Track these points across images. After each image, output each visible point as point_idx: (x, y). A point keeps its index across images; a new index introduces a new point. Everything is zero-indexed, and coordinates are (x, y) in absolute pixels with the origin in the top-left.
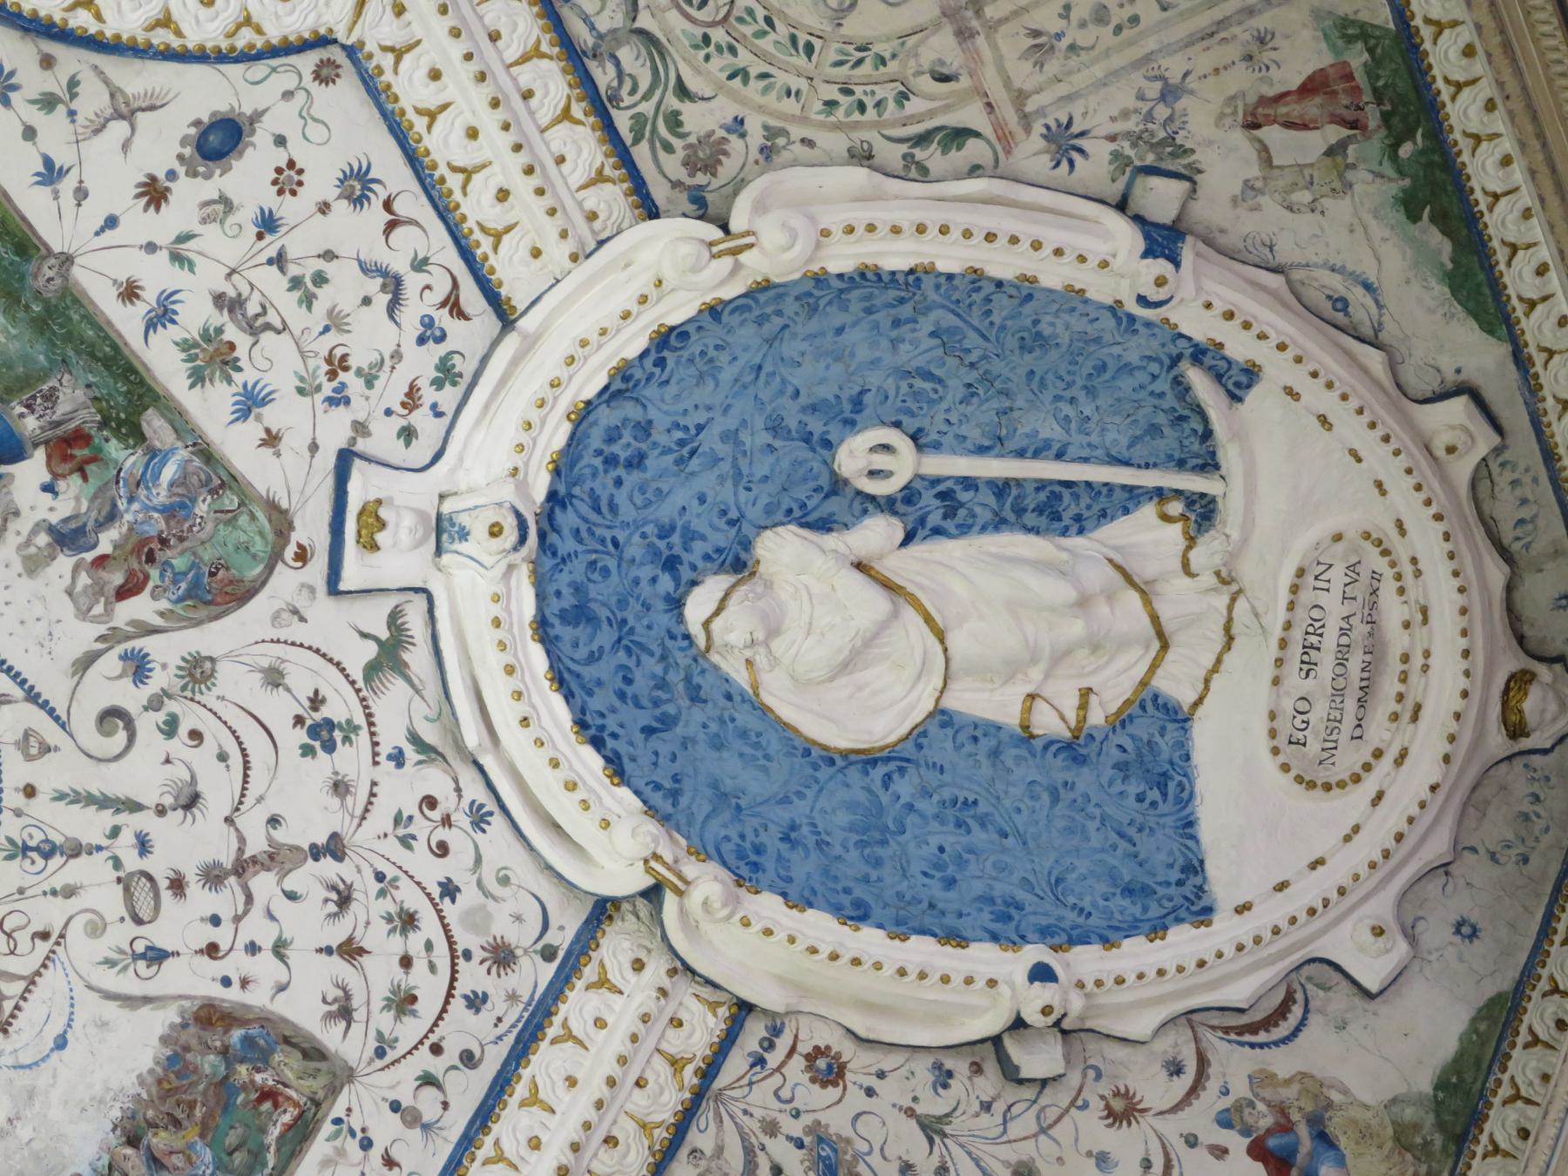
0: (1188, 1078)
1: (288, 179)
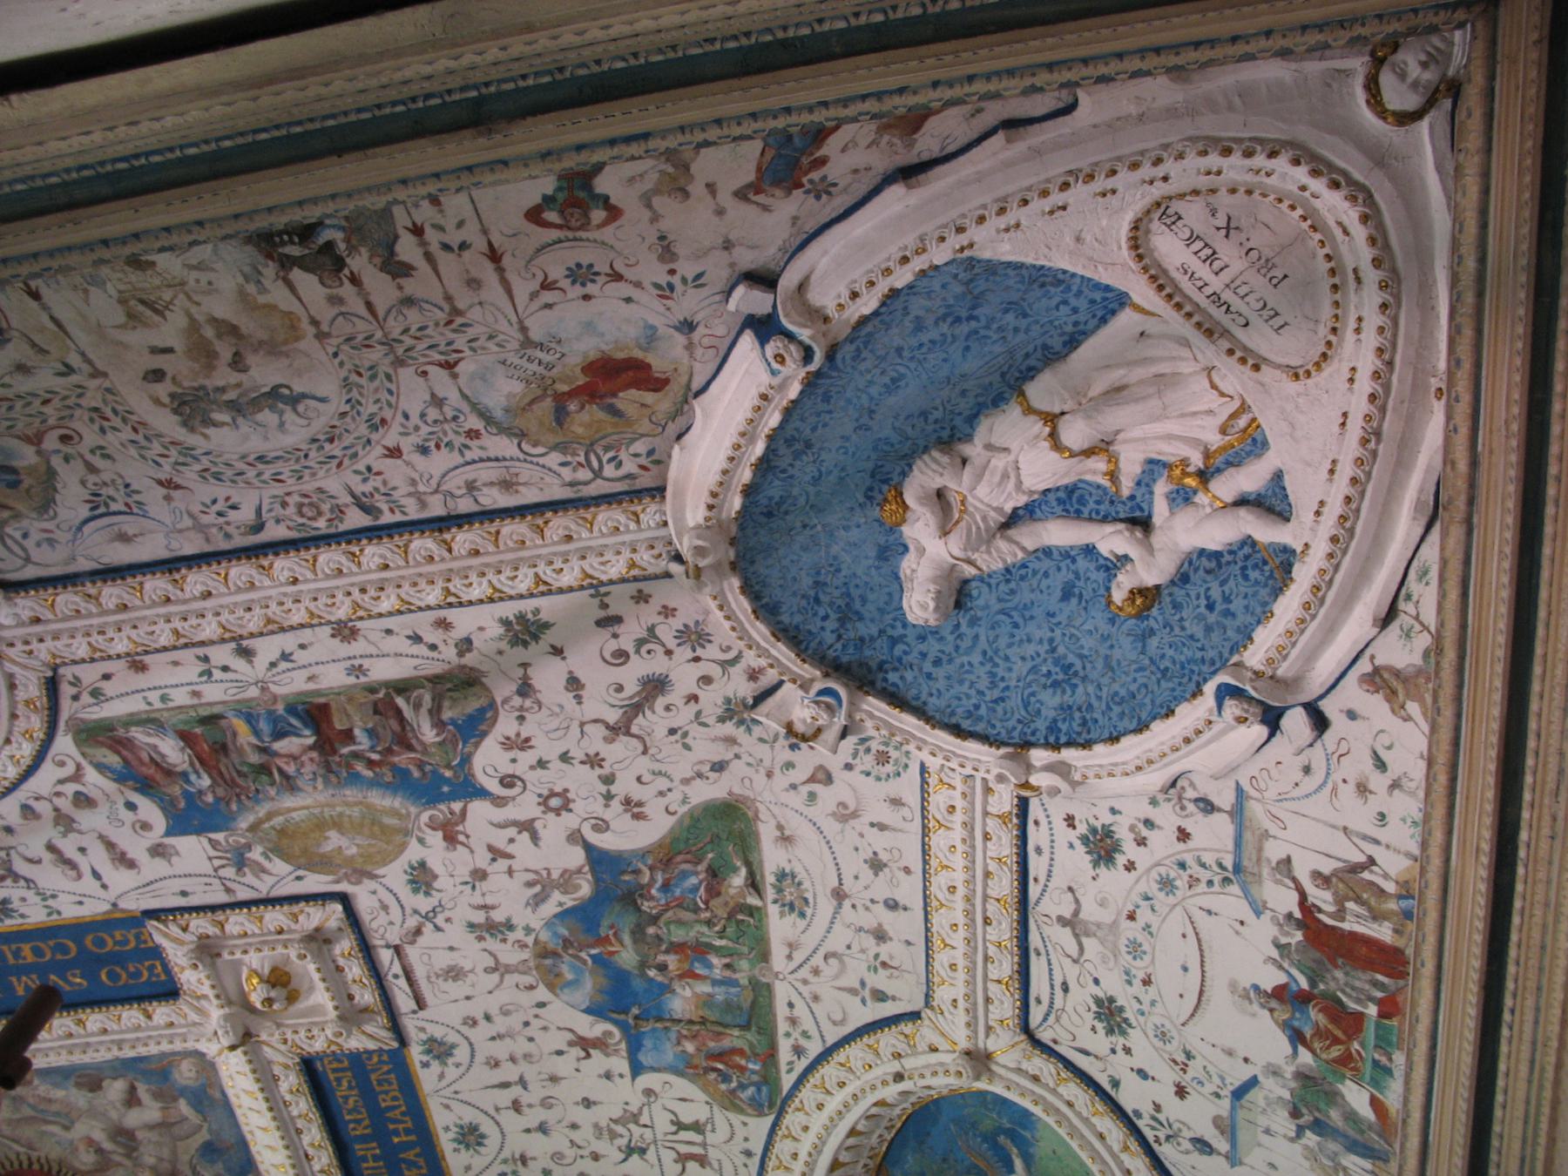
0: (462, 1069)
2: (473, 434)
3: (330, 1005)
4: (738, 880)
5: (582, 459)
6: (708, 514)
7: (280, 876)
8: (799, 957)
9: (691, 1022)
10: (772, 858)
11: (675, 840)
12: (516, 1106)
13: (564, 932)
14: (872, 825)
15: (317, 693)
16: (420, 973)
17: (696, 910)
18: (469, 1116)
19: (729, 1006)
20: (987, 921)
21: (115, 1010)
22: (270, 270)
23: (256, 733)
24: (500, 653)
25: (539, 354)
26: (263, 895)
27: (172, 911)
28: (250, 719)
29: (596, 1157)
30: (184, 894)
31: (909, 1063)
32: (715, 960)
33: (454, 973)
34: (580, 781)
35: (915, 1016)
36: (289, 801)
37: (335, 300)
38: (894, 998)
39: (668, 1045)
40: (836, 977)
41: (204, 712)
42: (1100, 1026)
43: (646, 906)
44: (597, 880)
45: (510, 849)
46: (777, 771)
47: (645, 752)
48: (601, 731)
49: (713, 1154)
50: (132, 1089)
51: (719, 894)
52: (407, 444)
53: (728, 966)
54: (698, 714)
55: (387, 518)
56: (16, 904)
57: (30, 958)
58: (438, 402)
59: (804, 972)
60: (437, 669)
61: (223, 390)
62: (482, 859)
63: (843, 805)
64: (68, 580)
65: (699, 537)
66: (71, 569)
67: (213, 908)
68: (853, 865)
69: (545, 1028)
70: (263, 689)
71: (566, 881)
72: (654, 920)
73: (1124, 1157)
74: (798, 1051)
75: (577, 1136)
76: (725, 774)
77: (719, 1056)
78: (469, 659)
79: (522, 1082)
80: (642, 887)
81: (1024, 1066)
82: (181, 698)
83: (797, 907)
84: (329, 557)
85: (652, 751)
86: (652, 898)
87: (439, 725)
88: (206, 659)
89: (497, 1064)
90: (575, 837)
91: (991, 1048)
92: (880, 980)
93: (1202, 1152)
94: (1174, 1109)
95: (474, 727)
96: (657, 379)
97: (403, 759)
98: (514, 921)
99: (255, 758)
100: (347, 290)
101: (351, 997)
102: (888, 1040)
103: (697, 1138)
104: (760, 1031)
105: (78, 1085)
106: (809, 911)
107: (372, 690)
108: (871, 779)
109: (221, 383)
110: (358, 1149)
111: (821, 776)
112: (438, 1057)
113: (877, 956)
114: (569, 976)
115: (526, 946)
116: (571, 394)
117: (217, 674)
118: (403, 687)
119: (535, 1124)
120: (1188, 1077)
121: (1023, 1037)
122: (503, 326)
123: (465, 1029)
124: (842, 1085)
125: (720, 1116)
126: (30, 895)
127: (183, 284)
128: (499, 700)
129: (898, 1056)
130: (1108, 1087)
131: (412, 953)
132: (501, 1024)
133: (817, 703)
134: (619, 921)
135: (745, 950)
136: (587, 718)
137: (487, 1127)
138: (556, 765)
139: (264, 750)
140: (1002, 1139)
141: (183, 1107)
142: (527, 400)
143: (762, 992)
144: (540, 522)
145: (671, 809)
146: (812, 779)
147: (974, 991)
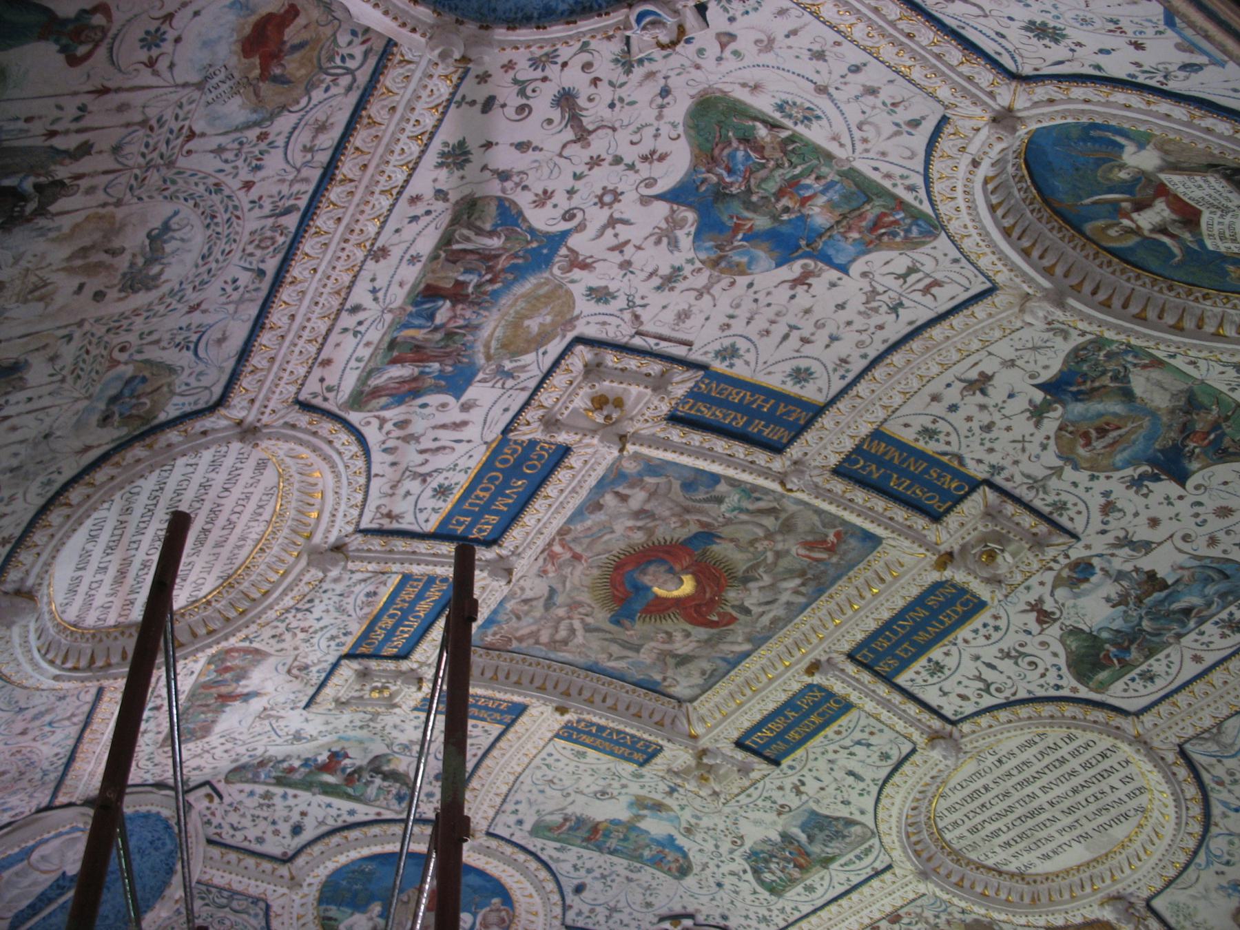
0: (753, 350)
1: (276, 833)
2: (262, 137)
3: (641, 388)
4: (762, 131)
5: (329, 78)
6: (420, 32)
7: (534, 363)
8: (846, 140)
9: (838, 222)
10: (763, 103)
11: (699, 146)
12: (805, 341)
13: (709, 244)
14: (787, 36)
15: (414, 286)
16: (666, 332)
17: (763, 166)
18: (788, 367)
19: (847, 198)
20: (909, 36)
21: (554, 479)
22: (42, 222)
23: (420, 327)
24: (463, 178)
25: (216, 80)
26: (541, 375)
27: (512, 422)
28: (406, 326)
29: (881, 327)
30: (506, 410)
31: (973, 148)
32: (808, 181)
33: (683, 316)
34: (602, 177)
35: (944, 120)
36: (485, 333)
37: (91, 190)
38: (923, 118)
39: (842, 244)
40: (879, 134)
41: (385, 345)
42: (1047, 41)
43: (734, 190)
44: (690, 206)
45: (622, 239)
46: (699, 61)
47: (614, 129)
48: (577, 147)
49: (939, 276)
50: (617, 494)
51: (763, 147)
52: (245, 175)
53: (818, 178)
54: (611, 84)
55: (303, 203)
56: (447, 483)
57: (487, 495)
58: (220, 150)
59: (860, 147)
60: (446, 219)
61: (132, 265)
62: (616, 258)
63: (757, 42)
64: (234, 377)
65: (432, 49)
66: (228, 371)
67: (527, 404)
68: (809, 67)
69: (769, 293)
70: (390, 311)
71: (674, 222)
72: (749, 191)
73: (1154, 108)
74: (911, 188)
75: (855, 327)
76: (675, 92)
77: (876, 225)
78: (454, 197)
79: (793, 328)
80: (718, 184)
81: (1035, 99)
82: (365, 353)
83: (809, 116)
84: (309, 245)
85: (617, 125)
86: (732, 184)
87: (492, 234)
88: (345, 330)
89: (768, 332)
90: (645, 201)
91: (1006, 104)
92: (903, 115)
93: (1196, 71)
94: (1148, 59)
95: (509, 216)
96: (287, 12)
97: (502, 263)
98: (677, 264)
99: (438, 336)
100: (84, 183)
101: (648, 375)
102: (946, 144)
103: (920, 275)
104: (879, 195)
105: (591, 513)
106: (819, 113)
107: (434, 257)
108: (752, 14)
109: (127, 264)
110: (753, 429)
111: (724, 39)
112: (732, 356)
113: (884, 104)
114: (745, 260)
115: (700, 270)
116: (265, 68)
117: (362, 329)
118: (446, 240)
119: (827, 341)
120: (1130, 34)
121: (1014, 84)
122: (175, 97)
123: (727, 333)
124: (953, 189)
125: (917, 255)
126: (445, 474)
127: (28, 270)
128: (500, 194)
129: (963, 149)
130: (1097, 73)
131: (648, 327)
132: (743, 313)
133: (644, 28)
134: (727, 213)
135: (815, 162)
136: (558, 149)
137: (803, 364)
138: (578, 185)
139: (436, 329)
140: (1092, 133)
141: (650, 480)
142: (253, 98)
143: (851, 174)
144: (365, 121)
145: (674, 135)
146: (723, 46)
147: (954, 82)
